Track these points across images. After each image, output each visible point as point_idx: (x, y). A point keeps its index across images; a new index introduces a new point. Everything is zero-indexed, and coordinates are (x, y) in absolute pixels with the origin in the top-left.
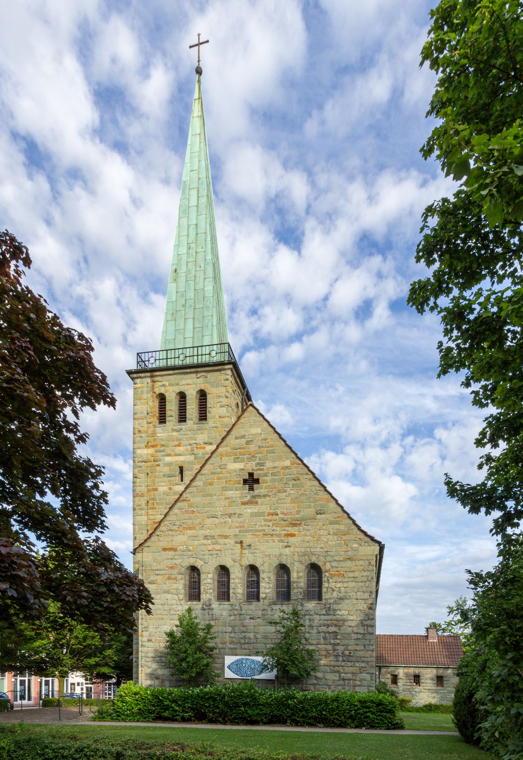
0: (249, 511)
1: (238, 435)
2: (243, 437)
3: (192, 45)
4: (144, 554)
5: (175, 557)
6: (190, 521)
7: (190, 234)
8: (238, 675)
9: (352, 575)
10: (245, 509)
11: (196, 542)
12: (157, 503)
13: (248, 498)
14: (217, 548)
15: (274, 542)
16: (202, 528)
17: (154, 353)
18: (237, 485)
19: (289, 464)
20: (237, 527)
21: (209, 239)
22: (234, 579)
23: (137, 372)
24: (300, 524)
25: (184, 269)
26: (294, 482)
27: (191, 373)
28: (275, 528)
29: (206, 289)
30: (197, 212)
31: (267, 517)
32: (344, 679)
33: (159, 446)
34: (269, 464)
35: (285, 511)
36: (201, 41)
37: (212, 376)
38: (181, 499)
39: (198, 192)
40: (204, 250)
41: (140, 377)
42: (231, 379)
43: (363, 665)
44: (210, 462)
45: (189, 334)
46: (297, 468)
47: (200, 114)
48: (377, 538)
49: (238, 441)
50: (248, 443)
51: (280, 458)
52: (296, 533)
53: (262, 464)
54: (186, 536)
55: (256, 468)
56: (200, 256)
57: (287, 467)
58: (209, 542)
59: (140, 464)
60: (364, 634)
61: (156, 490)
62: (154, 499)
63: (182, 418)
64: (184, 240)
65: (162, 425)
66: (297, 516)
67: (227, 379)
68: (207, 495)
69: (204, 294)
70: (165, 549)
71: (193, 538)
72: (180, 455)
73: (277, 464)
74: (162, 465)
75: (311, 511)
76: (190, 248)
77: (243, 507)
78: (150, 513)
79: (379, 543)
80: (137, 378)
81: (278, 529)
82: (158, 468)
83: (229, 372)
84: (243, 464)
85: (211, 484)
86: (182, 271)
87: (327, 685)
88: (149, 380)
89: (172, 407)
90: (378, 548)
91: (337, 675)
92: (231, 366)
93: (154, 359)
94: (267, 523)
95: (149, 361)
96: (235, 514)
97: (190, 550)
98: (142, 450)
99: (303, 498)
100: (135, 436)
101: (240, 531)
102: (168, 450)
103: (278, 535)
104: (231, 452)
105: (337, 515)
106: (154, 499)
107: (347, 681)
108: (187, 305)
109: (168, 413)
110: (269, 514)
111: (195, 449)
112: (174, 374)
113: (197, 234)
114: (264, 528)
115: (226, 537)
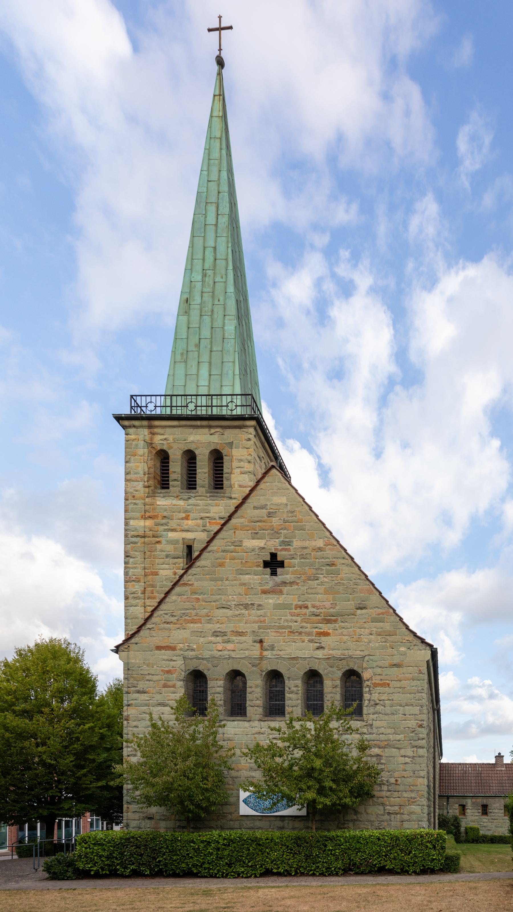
0: (271, 601)
1: (256, 504)
3: (211, 27)
4: (131, 653)
5: (174, 658)
6: (194, 612)
7: (207, 258)
8: (256, 811)
9: (398, 684)
10: (266, 599)
11: (202, 639)
13: (271, 584)
14: (228, 648)
15: (303, 642)
16: (209, 621)
17: (153, 398)
18: (256, 568)
19: (322, 546)
20: (254, 622)
21: (230, 267)
22: (251, 687)
23: (128, 418)
24: (335, 621)
25: (197, 299)
26: (328, 568)
28: (304, 624)
29: (226, 328)
30: (216, 232)
31: (294, 611)
32: (389, 813)
33: (160, 518)
34: (296, 543)
35: (317, 604)
36: (222, 26)
37: (230, 435)
38: (181, 582)
39: (218, 208)
40: (224, 280)
41: (134, 426)
42: (254, 439)
43: (413, 795)
44: (220, 536)
45: (203, 381)
47: (221, 114)
48: (429, 640)
49: (257, 512)
50: (270, 515)
51: (311, 537)
52: (330, 631)
53: (289, 544)
54: (188, 631)
55: (280, 548)
56: (219, 287)
57: (320, 549)
58: (219, 639)
59: (134, 539)
60: (413, 757)
61: (156, 574)
62: (153, 586)
63: (191, 484)
64: (198, 266)
65: (164, 491)
66: (332, 610)
67: (249, 440)
68: (215, 580)
69: (224, 335)
70: (159, 648)
71: (199, 634)
72: (188, 531)
73: (307, 544)
74: (164, 542)
75: (351, 605)
76: (206, 276)
77: (264, 596)
78: (147, 604)
79: (431, 646)
80: (130, 427)
81: (309, 625)
82: (158, 546)
83: (252, 430)
84: (264, 541)
85: (221, 565)
86: (195, 302)
87: (368, 821)
88: (146, 431)
89: (177, 469)
90: (429, 652)
91: (381, 808)
92: (253, 423)
93: (153, 405)
94: (294, 618)
95: (146, 407)
96: (253, 604)
97: (193, 650)
98: (136, 521)
100: (128, 502)
101: (260, 628)
102: (173, 524)
103: (309, 634)
104: (248, 526)
105: (380, 611)
107: (393, 816)
108: (202, 346)
109: (172, 476)
110: (297, 607)
111: (208, 524)
113: (216, 259)
114: (290, 624)
115: (241, 634)
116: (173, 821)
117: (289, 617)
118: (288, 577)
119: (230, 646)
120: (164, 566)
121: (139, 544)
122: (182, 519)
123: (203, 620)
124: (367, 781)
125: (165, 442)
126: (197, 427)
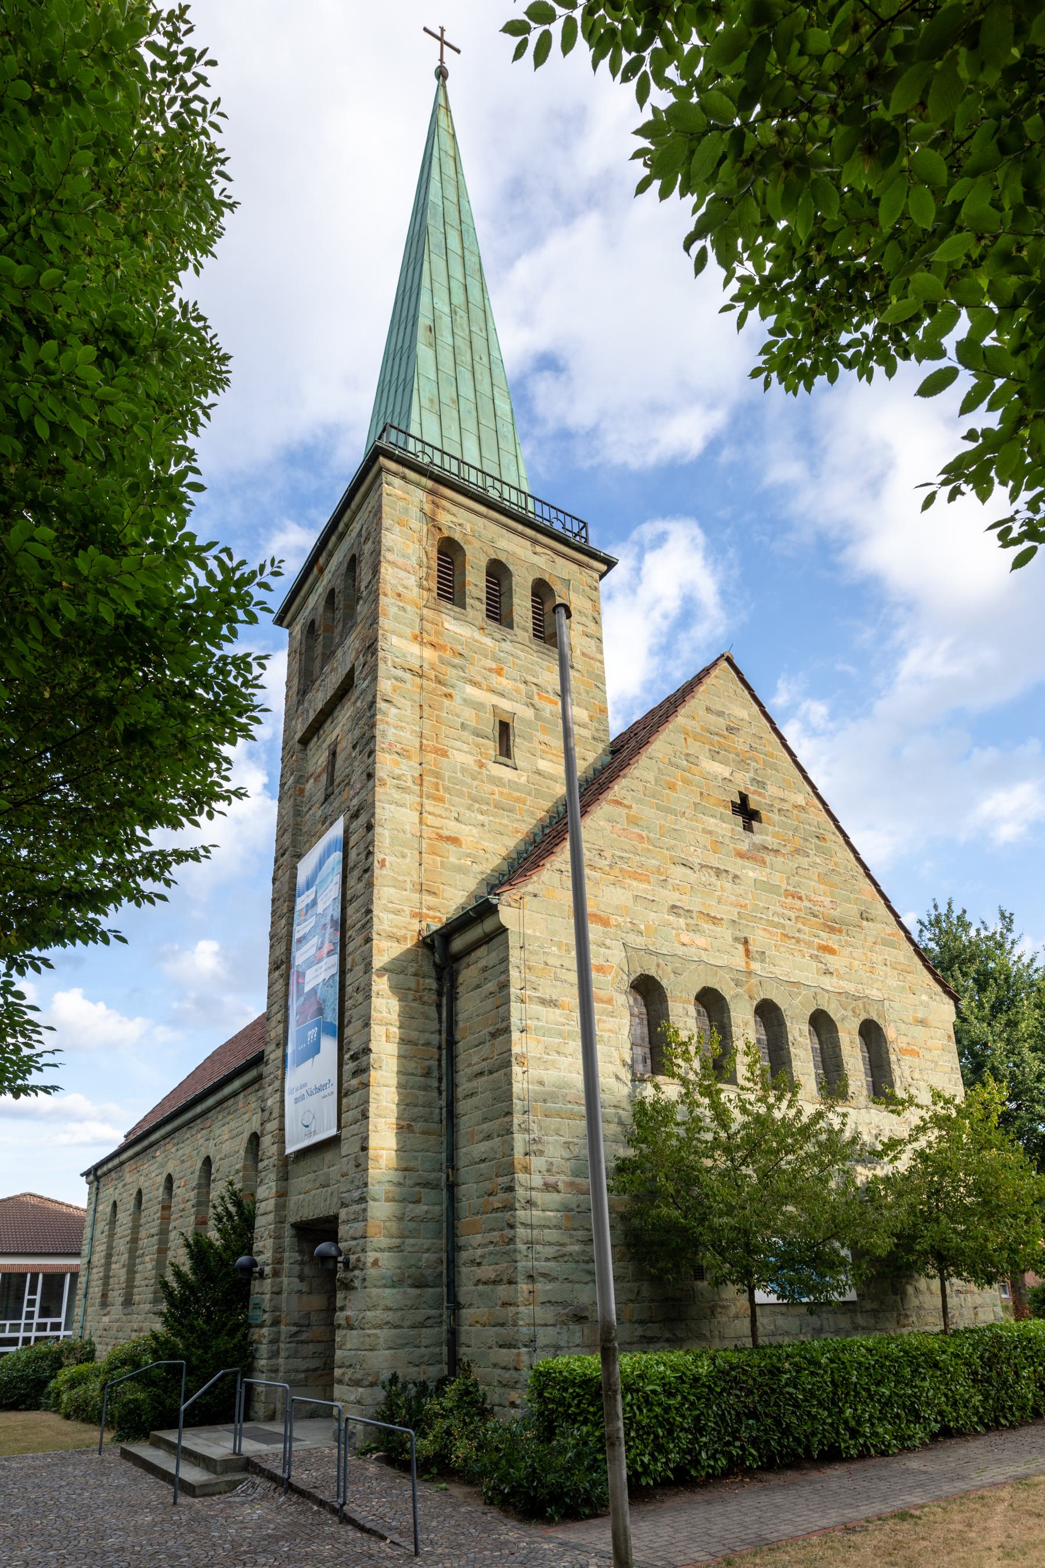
2: (720, 714)
7: (462, 291)
12: (447, 789)
27: (522, 535)
41: (404, 478)
46: (817, 815)
52: (836, 947)
58: (682, 921)
61: (444, 754)
68: (667, 810)
73: (786, 794)
74: (458, 699)
77: (739, 861)
78: (427, 808)
82: (446, 702)
98: (405, 642)
99: (836, 879)
103: (809, 944)
106: (437, 775)
110: (788, 894)
112: (486, 517)
115: (715, 920)
116: (627, 1325)
117: (780, 910)
118: (770, 841)
119: (701, 941)
120: (458, 744)
121: (408, 686)
122: (490, 670)
123: (653, 878)
124: (357, 1283)
125: (458, 528)
126: (514, 531)
